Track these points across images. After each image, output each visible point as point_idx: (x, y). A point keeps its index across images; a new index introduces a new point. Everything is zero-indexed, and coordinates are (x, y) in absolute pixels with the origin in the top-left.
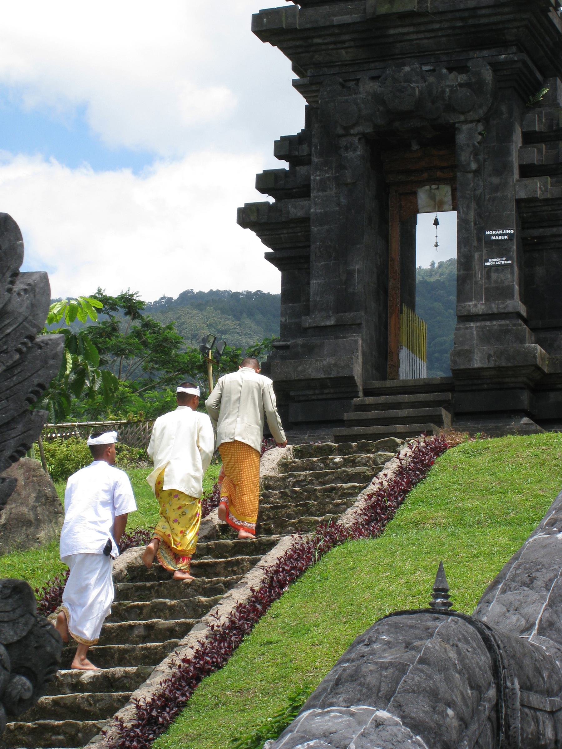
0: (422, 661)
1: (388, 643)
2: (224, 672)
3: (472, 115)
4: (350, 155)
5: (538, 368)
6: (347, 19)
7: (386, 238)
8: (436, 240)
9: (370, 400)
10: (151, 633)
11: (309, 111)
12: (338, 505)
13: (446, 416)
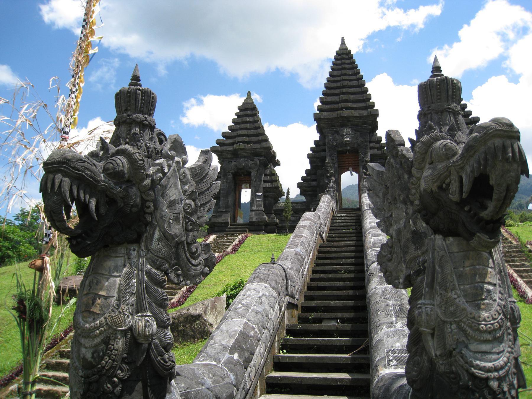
6: (230, 149)
7: (236, 194)
8: (246, 196)
13: (247, 230)
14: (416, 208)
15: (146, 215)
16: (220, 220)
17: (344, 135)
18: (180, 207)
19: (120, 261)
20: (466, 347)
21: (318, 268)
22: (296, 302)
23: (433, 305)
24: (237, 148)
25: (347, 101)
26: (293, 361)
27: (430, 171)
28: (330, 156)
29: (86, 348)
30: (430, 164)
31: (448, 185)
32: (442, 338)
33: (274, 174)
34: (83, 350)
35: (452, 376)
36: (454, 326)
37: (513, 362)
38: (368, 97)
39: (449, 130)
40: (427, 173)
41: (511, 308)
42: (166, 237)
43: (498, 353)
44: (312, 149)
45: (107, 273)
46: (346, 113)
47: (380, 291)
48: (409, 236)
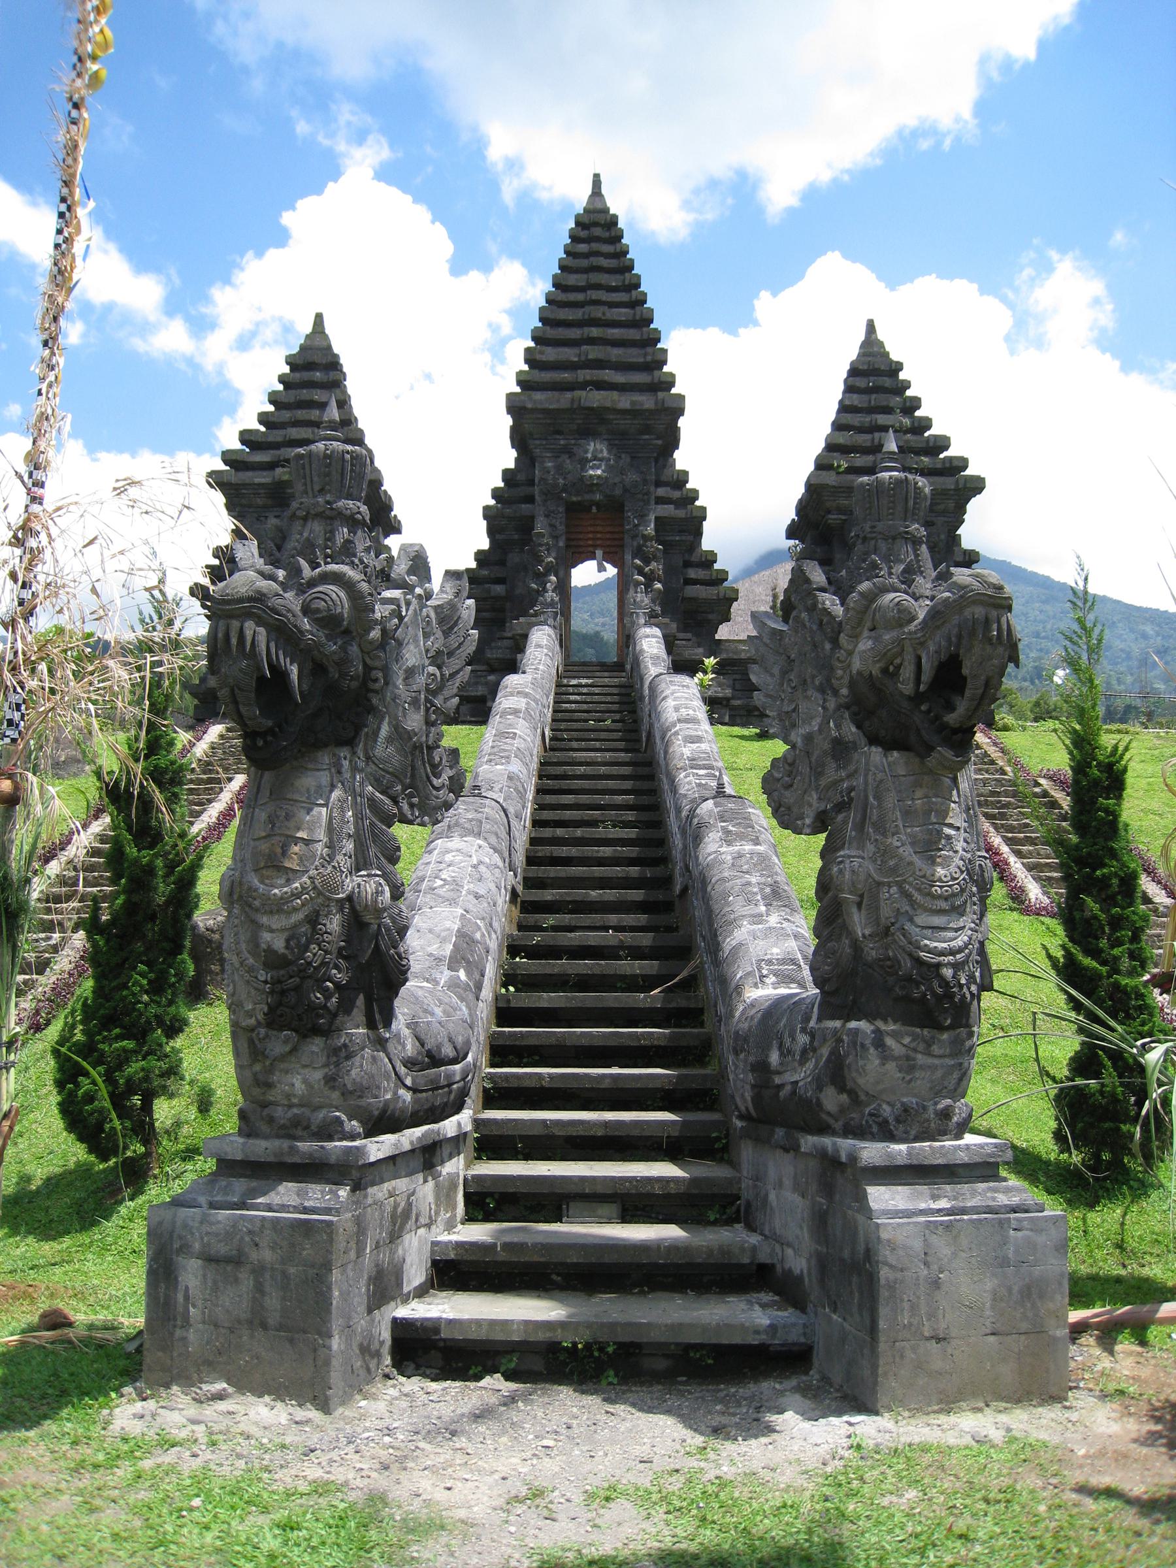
6: (263, 481)
14: (843, 700)
15: (371, 695)
17: (587, 461)
18: (421, 680)
19: (324, 778)
20: (911, 920)
21: (547, 815)
23: (863, 858)
25: (600, 364)
26: (538, 1005)
27: (870, 642)
28: (547, 516)
29: (272, 931)
30: (871, 630)
31: (898, 667)
32: (875, 909)
34: (266, 936)
35: (888, 963)
36: (894, 889)
37: (977, 945)
38: (659, 357)
39: (904, 571)
40: (865, 645)
41: (980, 865)
42: (400, 735)
43: (956, 930)
44: (496, 494)
45: (303, 799)
46: (595, 398)
47: (729, 857)
48: (827, 746)
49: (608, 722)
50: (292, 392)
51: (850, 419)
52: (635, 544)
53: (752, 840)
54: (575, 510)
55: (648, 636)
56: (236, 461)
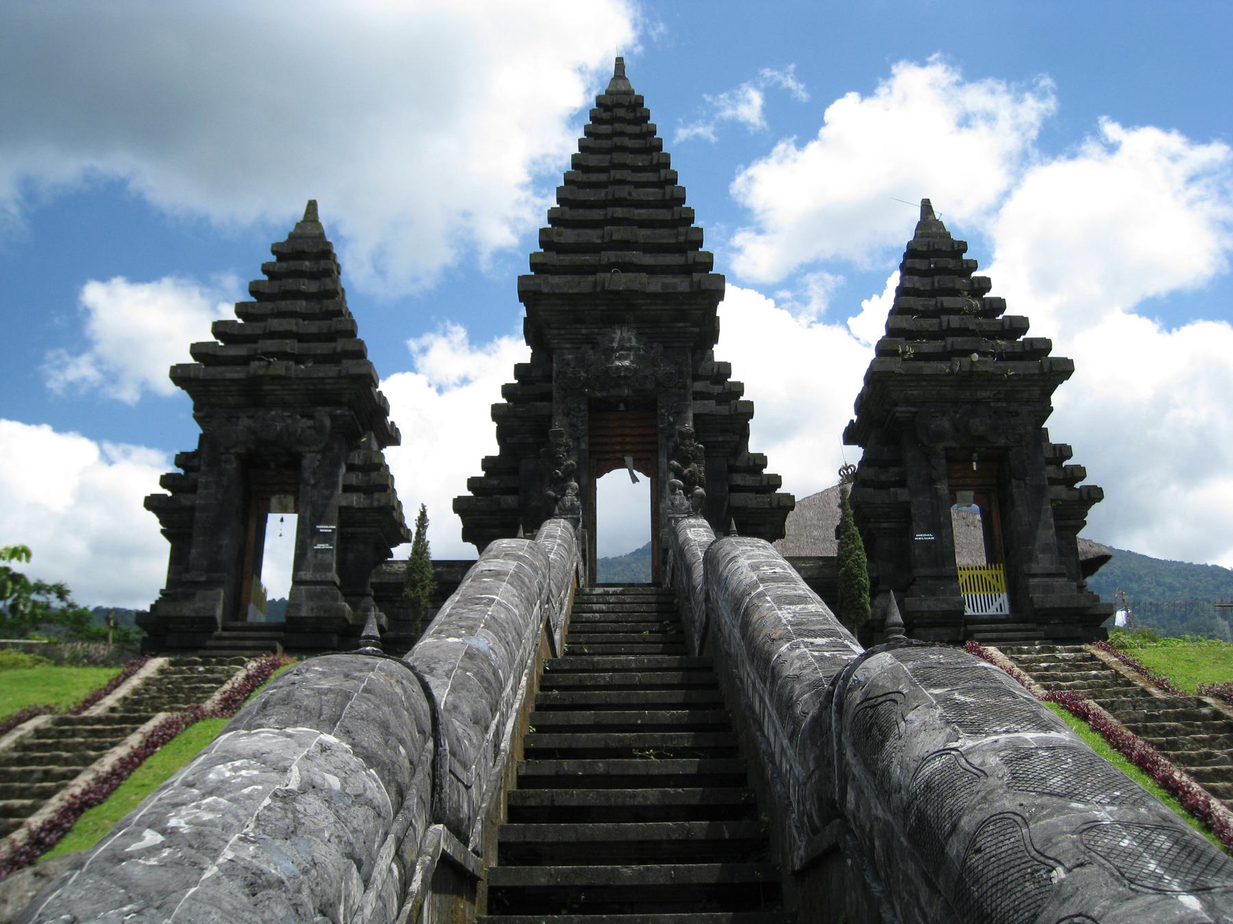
0: (366, 690)
1: (323, 673)
2: (105, 806)
3: (315, 448)
4: (228, 466)
5: (345, 620)
6: (236, 376)
9: (226, 634)
10: (47, 776)
11: (202, 437)
12: (199, 698)
13: (279, 647)
16: (187, 609)
17: (613, 351)
21: (548, 740)
22: (472, 863)
24: (261, 372)
28: (566, 414)
33: (381, 467)
46: (620, 281)
49: (646, 633)
50: (276, 283)
51: (912, 302)
52: (671, 444)
53: (1030, 721)
54: (598, 408)
55: (694, 526)
56: (207, 354)
